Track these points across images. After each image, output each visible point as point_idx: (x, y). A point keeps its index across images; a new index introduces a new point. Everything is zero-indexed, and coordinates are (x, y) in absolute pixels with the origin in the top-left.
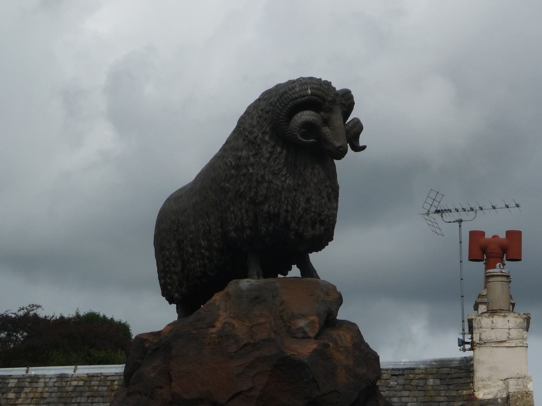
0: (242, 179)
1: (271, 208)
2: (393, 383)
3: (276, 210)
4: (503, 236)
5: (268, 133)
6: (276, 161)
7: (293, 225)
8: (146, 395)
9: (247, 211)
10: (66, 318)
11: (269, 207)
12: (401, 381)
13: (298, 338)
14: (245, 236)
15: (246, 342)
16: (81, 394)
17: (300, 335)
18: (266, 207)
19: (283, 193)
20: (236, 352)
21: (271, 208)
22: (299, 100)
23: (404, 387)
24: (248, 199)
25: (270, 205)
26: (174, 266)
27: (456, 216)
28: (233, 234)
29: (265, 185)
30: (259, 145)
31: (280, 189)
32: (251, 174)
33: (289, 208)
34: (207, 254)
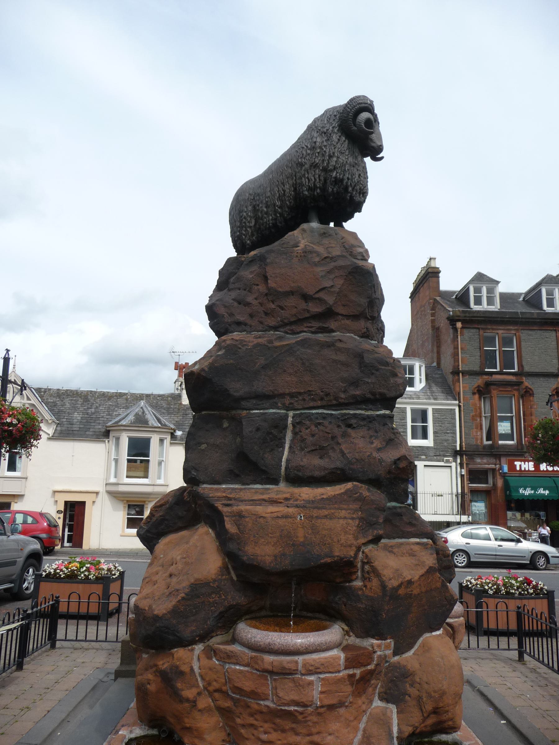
0: (317, 154)
1: (338, 174)
2: (158, 398)
3: (341, 176)
4: (184, 364)
5: (336, 127)
6: (342, 145)
7: (350, 189)
8: (245, 290)
9: (319, 176)
10: (373, 144)
11: (336, 174)
12: (161, 398)
13: (358, 260)
14: (316, 193)
15: (326, 255)
16: (64, 395)
17: (359, 257)
18: (335, 174)
19: (347, 166)
20: (319, 262)
21: (338, 174)
22: (363, 105)
23: (162, 400)
24: (321, 168)
25: (337, 173)
26: (249, 222)
27: (178, 354)
28: (306, 193)
29: (335, 159)
30: (330, 134)
31: (345, 163)
32: (324, 151)
33: (350, 177)
34: (279, 210)
